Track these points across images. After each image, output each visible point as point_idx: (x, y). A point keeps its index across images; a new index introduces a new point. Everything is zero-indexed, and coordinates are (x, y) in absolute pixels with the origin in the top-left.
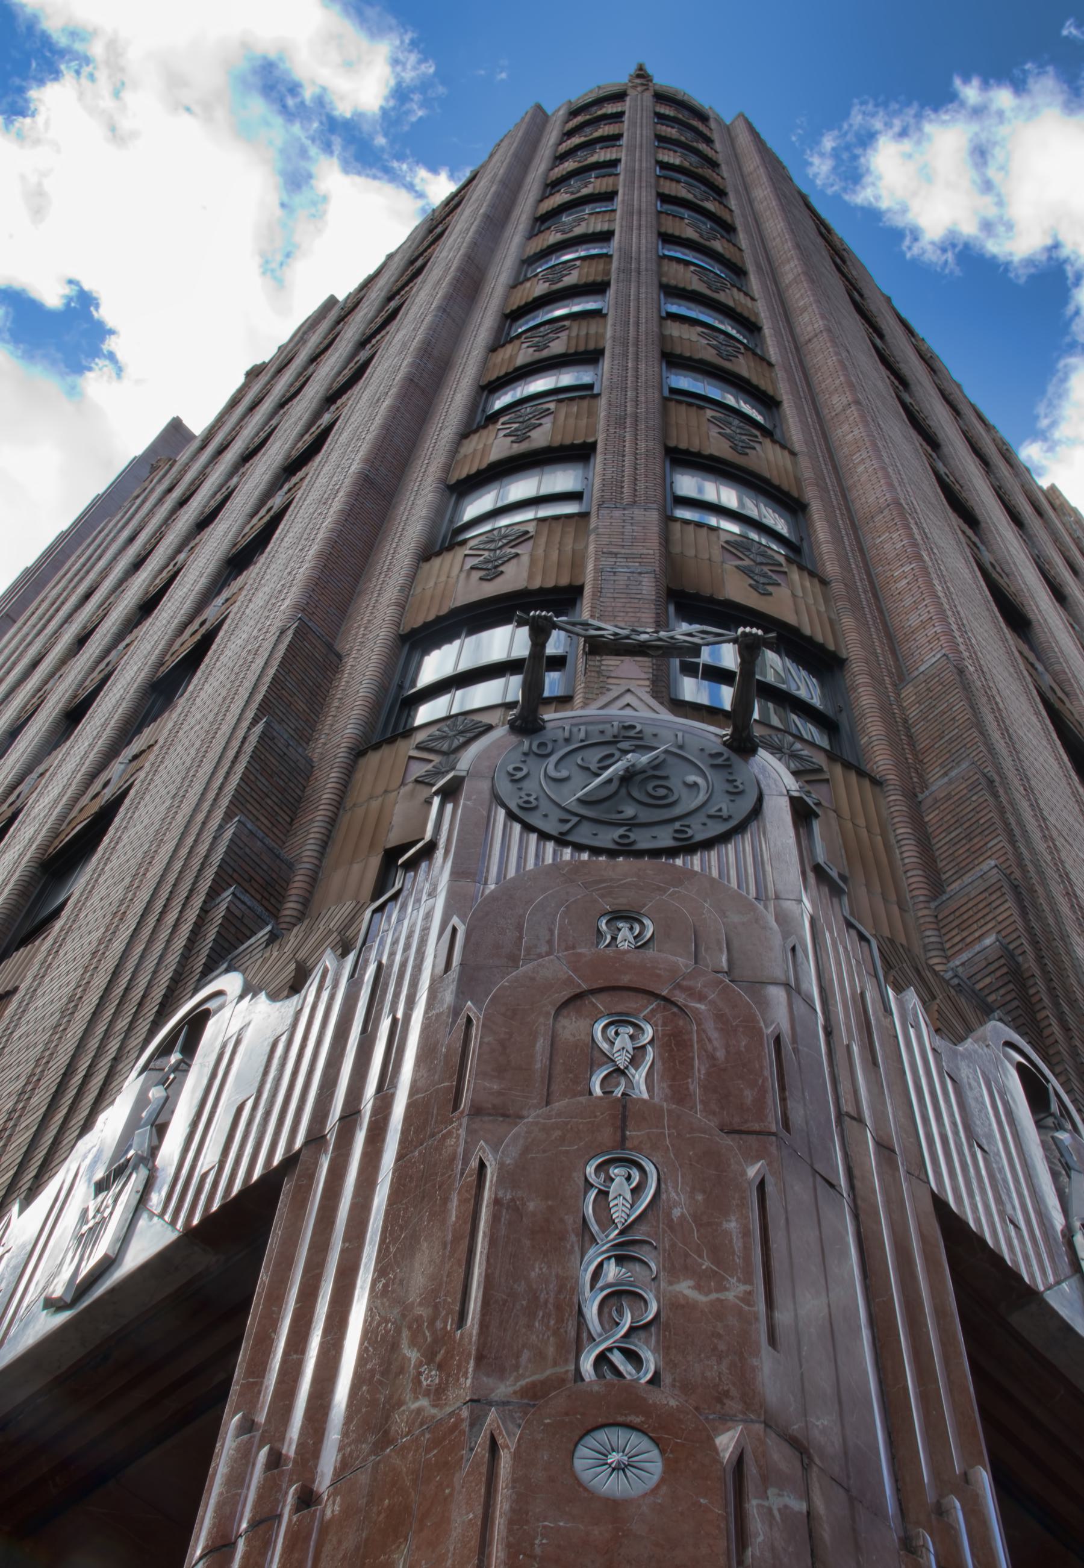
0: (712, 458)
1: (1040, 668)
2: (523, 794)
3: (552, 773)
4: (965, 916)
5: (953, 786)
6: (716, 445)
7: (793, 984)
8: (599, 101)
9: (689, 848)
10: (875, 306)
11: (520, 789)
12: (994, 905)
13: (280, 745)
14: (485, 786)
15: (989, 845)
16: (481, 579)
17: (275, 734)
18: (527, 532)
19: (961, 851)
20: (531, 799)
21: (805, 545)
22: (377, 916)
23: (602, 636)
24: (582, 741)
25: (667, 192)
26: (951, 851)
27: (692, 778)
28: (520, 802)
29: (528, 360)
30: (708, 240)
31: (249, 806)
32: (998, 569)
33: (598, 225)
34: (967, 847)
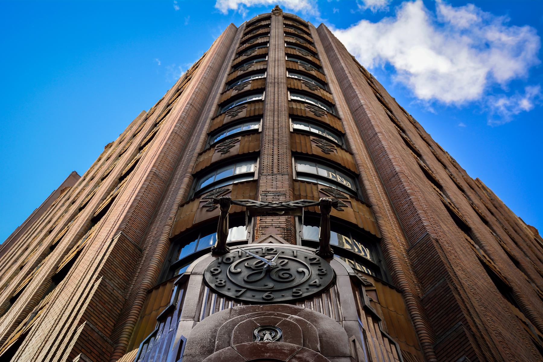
0: (313, 155)
1: (477, 247)
2: (218, 280)
3: (233, 270)
4: (449, 351)
5: (437, 291)
6: (315, 149)
7: (354, 356)
8: (259, 20)
9: (302, 300)
10: (387, 100)
11: (217, 278)
12: (463, 343)
13: (109, 289)
14: (200, 278)
15: (458, 317)
16: (207, 211)
17: (107, 284)
18: (229, 190)
19: (444, 321)
20: (222, 282)
21: (360, 192)
22: (146, 345)
23: (255, 206)
24: (247, 256)
25: (289, 52)
26: (439, 322)
27: (301, 269)
28: (217, 284)
29: (229, 121)
30: (309, 70)
31: (92, 318)
32: (453, 205)
33: (259, 67)
34: (447, 319)
